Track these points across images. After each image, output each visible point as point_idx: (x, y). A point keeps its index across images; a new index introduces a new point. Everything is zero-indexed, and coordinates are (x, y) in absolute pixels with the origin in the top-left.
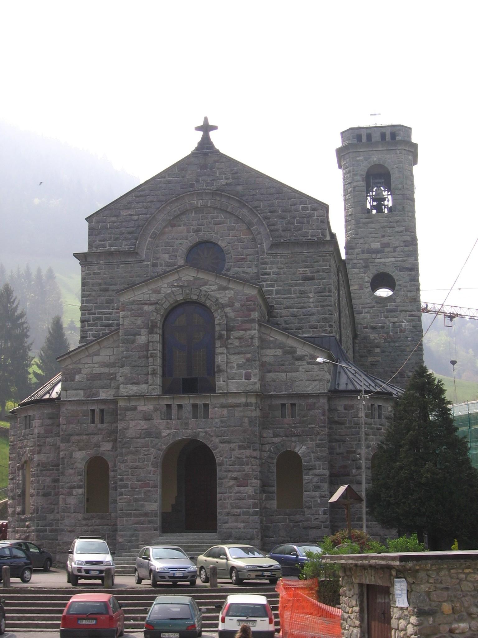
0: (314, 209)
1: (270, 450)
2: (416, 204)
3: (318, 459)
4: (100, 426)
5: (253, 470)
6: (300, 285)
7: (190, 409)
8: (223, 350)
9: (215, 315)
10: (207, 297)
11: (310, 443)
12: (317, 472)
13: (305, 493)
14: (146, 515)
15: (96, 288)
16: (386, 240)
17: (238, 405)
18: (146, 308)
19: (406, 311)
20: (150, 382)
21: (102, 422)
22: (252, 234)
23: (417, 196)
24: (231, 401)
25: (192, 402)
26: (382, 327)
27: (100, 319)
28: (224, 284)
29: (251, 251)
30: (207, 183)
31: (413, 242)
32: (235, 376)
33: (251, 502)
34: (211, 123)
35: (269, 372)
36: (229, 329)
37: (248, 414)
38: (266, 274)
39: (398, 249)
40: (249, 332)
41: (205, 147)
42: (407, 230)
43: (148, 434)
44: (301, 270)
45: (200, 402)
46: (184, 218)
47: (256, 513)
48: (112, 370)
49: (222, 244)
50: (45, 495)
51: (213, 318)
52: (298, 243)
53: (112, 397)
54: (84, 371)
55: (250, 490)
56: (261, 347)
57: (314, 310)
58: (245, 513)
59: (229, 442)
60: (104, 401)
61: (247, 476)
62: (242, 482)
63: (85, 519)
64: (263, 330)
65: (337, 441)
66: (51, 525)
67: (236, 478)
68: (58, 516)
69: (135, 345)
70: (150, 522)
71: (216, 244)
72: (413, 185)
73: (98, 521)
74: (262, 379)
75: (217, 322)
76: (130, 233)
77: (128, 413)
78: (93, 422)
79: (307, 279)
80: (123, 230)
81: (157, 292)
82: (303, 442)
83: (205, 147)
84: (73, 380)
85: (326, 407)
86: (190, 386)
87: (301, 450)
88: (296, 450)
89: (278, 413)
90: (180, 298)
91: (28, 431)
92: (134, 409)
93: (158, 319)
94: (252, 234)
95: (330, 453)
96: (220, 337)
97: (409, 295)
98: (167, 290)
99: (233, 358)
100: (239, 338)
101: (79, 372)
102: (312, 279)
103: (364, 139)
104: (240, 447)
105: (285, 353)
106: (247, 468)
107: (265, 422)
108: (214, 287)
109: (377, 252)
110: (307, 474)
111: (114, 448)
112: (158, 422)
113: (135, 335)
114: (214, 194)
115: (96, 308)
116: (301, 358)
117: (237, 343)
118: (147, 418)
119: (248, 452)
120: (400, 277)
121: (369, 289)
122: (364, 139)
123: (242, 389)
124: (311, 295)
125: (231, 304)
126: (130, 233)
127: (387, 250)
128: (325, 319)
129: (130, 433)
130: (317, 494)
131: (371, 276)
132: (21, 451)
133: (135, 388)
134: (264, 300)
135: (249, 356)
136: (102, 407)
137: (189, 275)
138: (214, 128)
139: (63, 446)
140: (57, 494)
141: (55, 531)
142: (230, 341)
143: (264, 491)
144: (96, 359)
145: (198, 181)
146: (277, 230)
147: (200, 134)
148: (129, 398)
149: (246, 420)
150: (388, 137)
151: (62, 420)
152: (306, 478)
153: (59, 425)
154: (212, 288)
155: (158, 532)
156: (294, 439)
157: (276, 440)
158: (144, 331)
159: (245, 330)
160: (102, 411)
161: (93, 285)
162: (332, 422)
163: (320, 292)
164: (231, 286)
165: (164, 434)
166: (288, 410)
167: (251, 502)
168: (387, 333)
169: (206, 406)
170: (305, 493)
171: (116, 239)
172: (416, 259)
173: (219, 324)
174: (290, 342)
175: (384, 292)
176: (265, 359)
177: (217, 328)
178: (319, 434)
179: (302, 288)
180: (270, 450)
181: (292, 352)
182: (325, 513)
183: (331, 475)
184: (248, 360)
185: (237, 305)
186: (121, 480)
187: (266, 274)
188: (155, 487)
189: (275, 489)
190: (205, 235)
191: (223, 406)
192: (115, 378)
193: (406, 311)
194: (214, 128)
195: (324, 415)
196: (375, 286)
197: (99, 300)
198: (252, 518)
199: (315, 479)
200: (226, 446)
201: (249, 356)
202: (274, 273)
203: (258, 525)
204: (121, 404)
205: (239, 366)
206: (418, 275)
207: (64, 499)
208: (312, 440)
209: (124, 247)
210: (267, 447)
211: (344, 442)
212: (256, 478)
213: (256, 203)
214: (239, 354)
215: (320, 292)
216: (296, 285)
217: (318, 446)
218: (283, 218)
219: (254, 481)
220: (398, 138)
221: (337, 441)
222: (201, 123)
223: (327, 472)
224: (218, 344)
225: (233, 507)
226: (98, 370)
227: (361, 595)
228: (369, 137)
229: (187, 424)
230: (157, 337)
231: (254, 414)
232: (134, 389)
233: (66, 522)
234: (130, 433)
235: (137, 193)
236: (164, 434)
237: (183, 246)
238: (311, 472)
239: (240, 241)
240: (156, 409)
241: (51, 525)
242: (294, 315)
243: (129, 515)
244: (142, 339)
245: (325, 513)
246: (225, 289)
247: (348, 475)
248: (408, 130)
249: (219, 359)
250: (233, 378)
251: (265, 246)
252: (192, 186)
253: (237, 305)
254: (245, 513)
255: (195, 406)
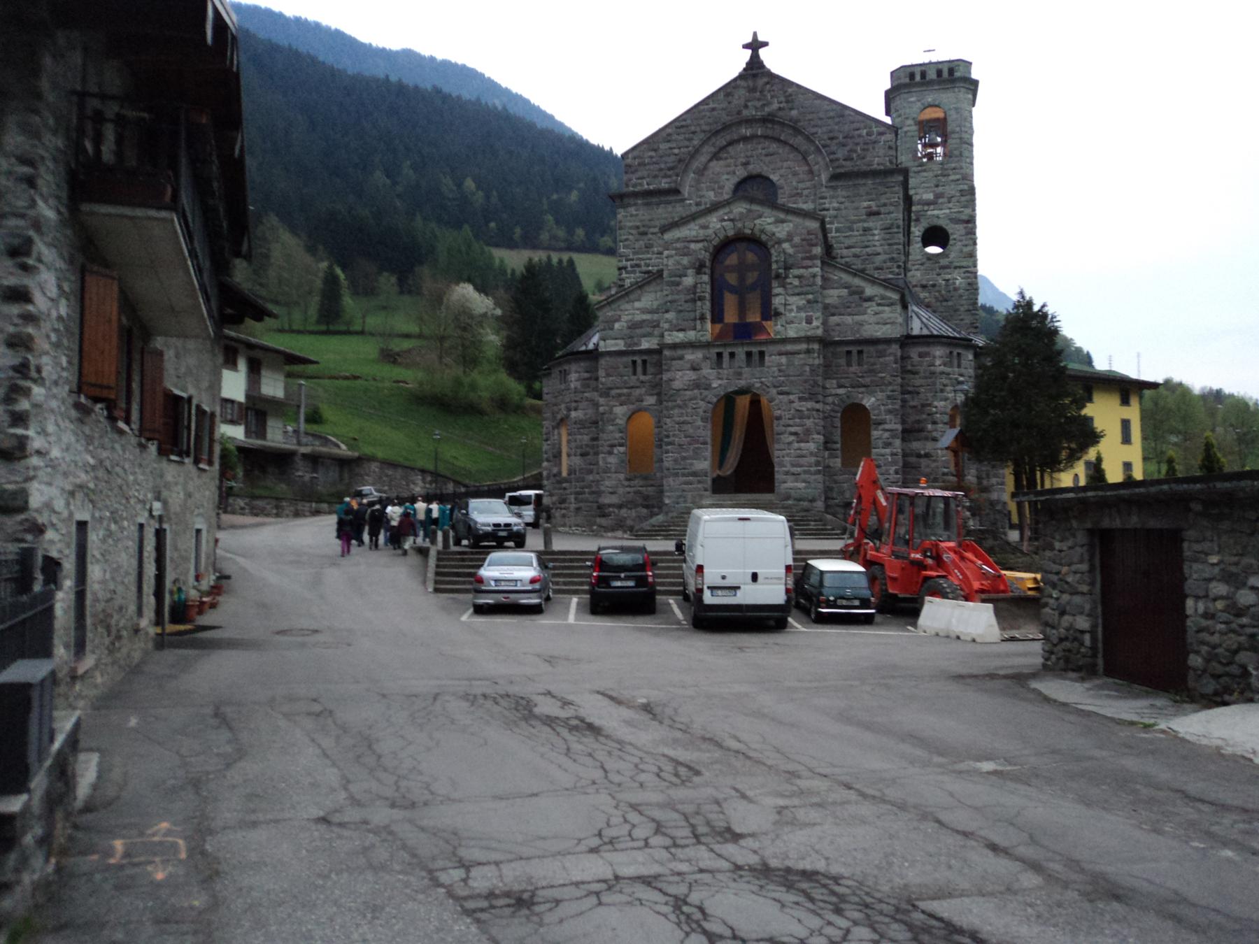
0: (881, 134)
1: (833, 403)
2: (975, 149)
3: (890, 412)
4: (642, 378)
5: (816, 424)
6: (864, 221)
7: (743, 357)
8: (780, 290)
9: (773, 251)
10: (762, 231)
11: (880, 395)
12: (887, 427)
13: (874, 451)
14: (694, 474)
15: (634, 232)
16: (940, 189)
17: (798, 353)
18: (693, 246)
19: (960, 267)
20: (699, 327)
21: (645, 373)
22: (808, 164)
23: (977, 140)
24: (789, 347)
25: (746, 349)
26: (934, 286)
27: (638, 266)
28: (782, 216)
29: (808, 184)
30: (756, 108)
31: (971, 191)
32: (795, 318)
33: (813, 459)
34: (761, 38)
35: (833, 315)
36: (787, 268)
37: (810, 361)
38: (824, 209)
39: (954, 200)
40: (811, 270)
41: (755, 67)
42: (964, 178)
43: (697, 385)
44: (866, 204)
45: (755, 350)
46: (730, 149)
47: (818, 472)
48: (656, 317)
49: (774, 178)
50: (582, 455)
51: (771, 255)
52: (865, 174)
53: (656, 347)
54: (624, 318)
55: (812, 446)
56: (823, 288)
57: (879, 249)
58: (805, 472)
59: (788, 393)
60: (649, 352)
61: (808, 432)
62: (803, 437)
63: (628, 480)
64: (826, 269)
65: (910, 393)
66: (589, 486)
67: (795, 434)
68: (598, 477)
69: (680, 288)
70: (699, 482)
71: (768, 179)
72: (971, 128)
73: (641, 483)
74: (825, 323)
75: (774, 259)
76: (670, 169)
77: (674, 362)
78: (635, 373)
79: (871, 214)
80: (663, 166)
81: (705, 227)
82: (872, 393)
83: (755, 67)
84: (612, 329)
85: (899, 354)
86: (744, 332)
87: (869, 402)
88: (864, 402)
89: (843, 361)
90: (731, 233)
91: (563, 387)
92: (681, 358)
93: (706, 256)
94: (808, 164)
95: (902, 406)
96: (778, 276)
97: (965, 250)
98: (717, 225)
99: (792, 299)
100: (799, 277)
101: (618, 320)
102: (878, 213)
103: (918, 78)
104: (801, 399)
105: (852, 293)
106: (809, 423)
107: (828, 370)
108: (769, 220)
109: (929, 203)
110: (876, 429)
111: (660, 402)
112: (707, 371)
113: (680, 276)
114: (765, 120)
115: (634, 253)
116: (870, 299)
117: (796, 282)
118: (694, 368)
119: (810, 404)
120: (955, 231)
121: (920, 245)
122: (918, 78)
123: (802, 334)
124: (876, 232)
125: (789, 238)
126: (670, 169)
127: (941, 200)
128: (892, 259)
129: (677, 384)
130: (888, 451)
131: (922, 230)
132: (555, 408)
133: (681, 335)
134: (825, 236)
135: (810, 297)
136: (645, 357)
137: (740, 208)
138: (765, 44)
139: (602, 401)
140: (597, 454)
141: (593, 493)
142: (788, 281)
143: (826, 449)
144: (637, 304)
145: (746, 107)
146: (837, 160)
147: (749, 52)
148: (675, 346)
149: (807, 369)
150: (945, 74)
151: (601, 373)
152: (875, 433)
153: (597, 379)
154: (768, 223)
155: (708, 493)
156: (861, 390)
157: (841, 391)
158: (690, 272)
159: (806, 267)
160: (644, 362)
161: (631, 228)
162: (904, 371)
163: (887, 229)
164: (790, 217)
165: (714, 385)
166: (855, 357)
167: (813, 459)
168: (939, 291)
169: (762, 354)
170: (874, 451)
171: (656, 177)
172: (974, 210)
173: (777, 262)
174: (857, 282)
175: (934, 250)
176: (827, 301)
177: (774, 266)
178: (890, 384)
179: (866, 225)
180: (833, 403)
181: (859, 292)
182: (897, 473)
183: (904, 431)
184: (809, 302)
185: (797, 240)
186: (668, 436)
187: (824, 209)
188: (705, 443)
189: (839, 446)
190: (755, 168)
191: (780, 354)
192: (658, 326)
193: (960, 267)
194: (765, 44)
195: (896, 363)
196: (927, 242)
197: (637, 246)
198: (813, 477)
199: (886, 435)
200: (784, 398)
201: (810, 297)
202: (835, 209)
203: (821, 486)
204: (667, 353)
205: (799, 309)
206: (975, 227)
207: (604, 459)
208: (882, 391)
209: (664, 184)
210: (830, 399)
211: (918, 393)
212: (819, 433)
213: (814, 130)
214: (798, 294)
215: (887, 229)
216: (860, 221)
217: (889, 397)
218: (844, 145)
219: (815, 436)
220: (957, 74)
221: (910, 393)
222: (749, 40)
223: (899, 427)
224: (775, 284)
225: (793, 466)
226: (640, 317)
227: (1091, 546)
228: (923, 75)
229: (740, 374)
230: (706, 278)
231: (817, 362)
232: (679, 337)
233: (607, 483)
234: (677, 384)
235: (677, 124)
236: (714, 385)
237: (729, 184)
238: (881, 427)
239: (795, 174)
240: (706, 358)
241: (589, 486)
242: (855, 256)
243: (676, 475)
244: (689, 281)
245: (897, 473)
246: (783, 221)
247: (921, 430)
248: (968, 64)
249: (777, 302)
250: (792, 322)
251: (824, 177)
252: (739, 113)
253: (797, 240)
254: (805, 472)
255: (749, 354)
